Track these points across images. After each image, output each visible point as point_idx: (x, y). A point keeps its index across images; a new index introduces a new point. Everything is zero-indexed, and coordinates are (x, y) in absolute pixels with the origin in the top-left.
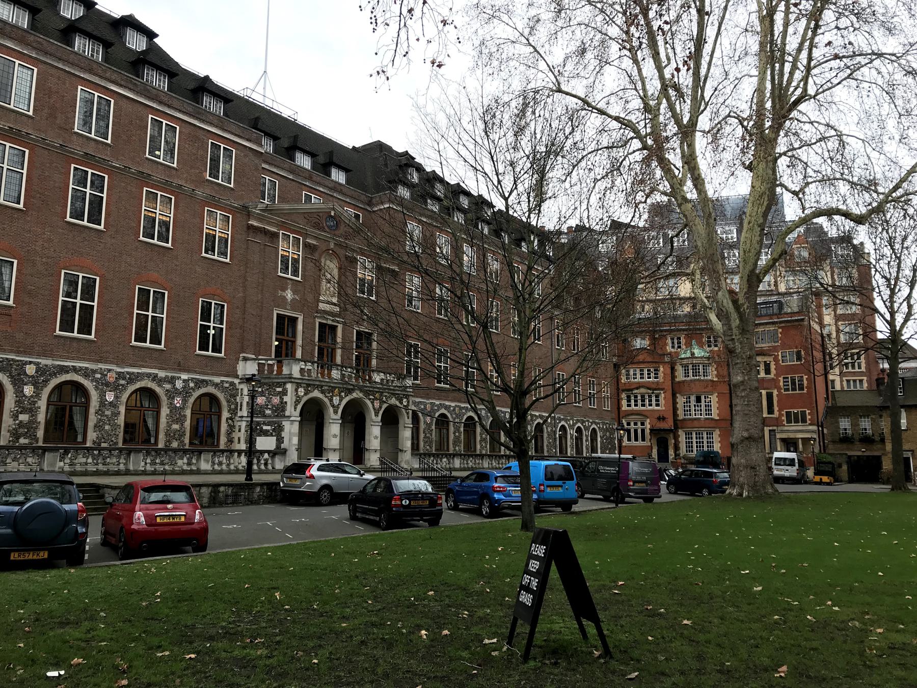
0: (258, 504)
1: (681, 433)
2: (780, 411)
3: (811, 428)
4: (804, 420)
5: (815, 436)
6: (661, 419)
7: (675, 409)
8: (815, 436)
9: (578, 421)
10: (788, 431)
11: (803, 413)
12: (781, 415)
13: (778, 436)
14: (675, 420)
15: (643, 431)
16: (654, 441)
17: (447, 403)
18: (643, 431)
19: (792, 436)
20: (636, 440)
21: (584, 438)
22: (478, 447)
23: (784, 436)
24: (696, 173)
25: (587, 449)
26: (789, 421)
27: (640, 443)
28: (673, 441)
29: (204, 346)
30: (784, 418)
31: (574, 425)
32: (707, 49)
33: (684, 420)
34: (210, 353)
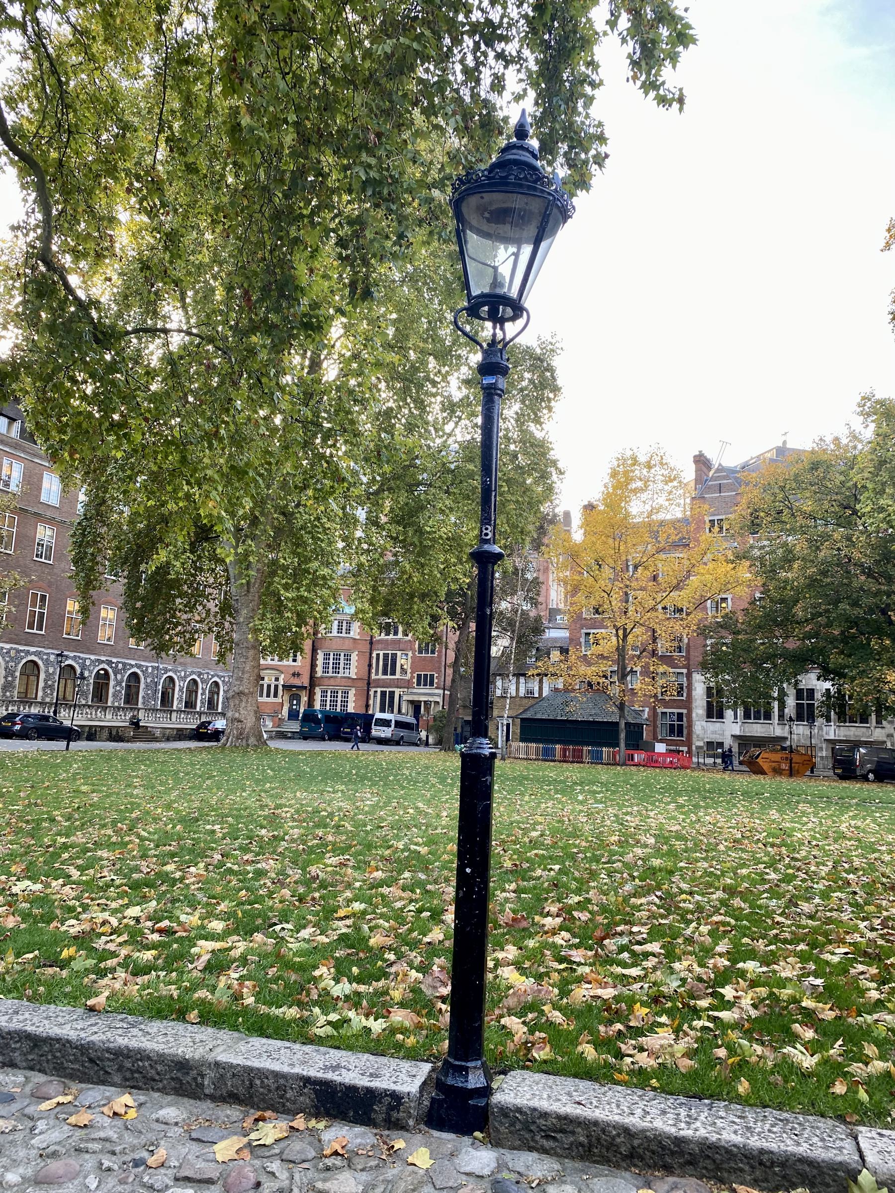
0: (324, 740)
1: (318, 691)
2: (412, 673)
3: (437, 691)
4: (432, 684)
5: (439, 700)
6: (296, 675)
7: (313, 666)
8: (439, 700)
9: (193, 673)
10: (412, 693)
11: (432, 676)
12: (412, 677)
13: (405, 698)
14: (312, 677)
15: (276, 687)
16: (286, 698)
17: (82, 655)
18: (276, 687)
19: (416, 698)
20: (268, 696)
21: (200, 691)
22: (40, 694)
23: (410, 698)
24: (612, 1146)
25: (202, 703)
26: (419, 684)
27: (272, 699)
28: (306, 699)
29: (31, 626)
30: (415, 680)
31: (185, 677)
32: (517, 190)
33: (322, 677)
34: (35, 631)
